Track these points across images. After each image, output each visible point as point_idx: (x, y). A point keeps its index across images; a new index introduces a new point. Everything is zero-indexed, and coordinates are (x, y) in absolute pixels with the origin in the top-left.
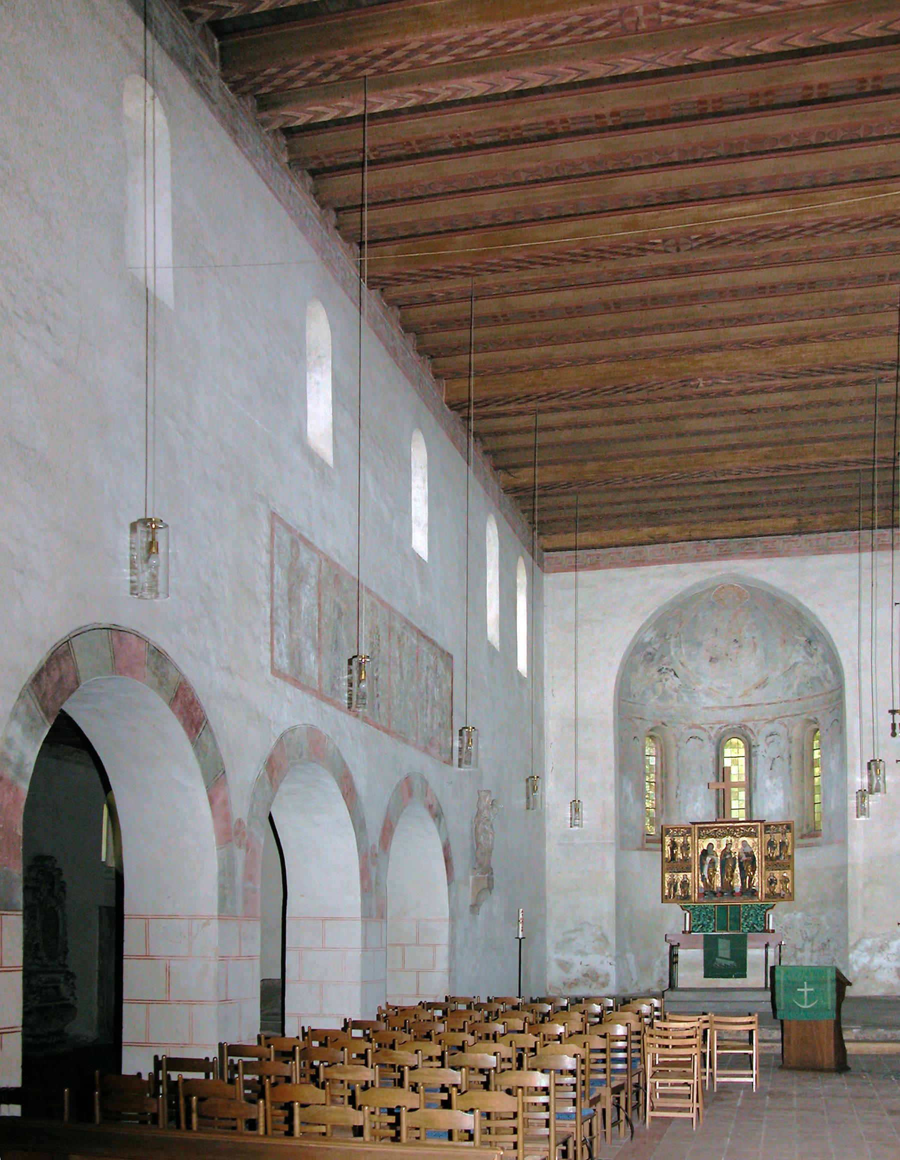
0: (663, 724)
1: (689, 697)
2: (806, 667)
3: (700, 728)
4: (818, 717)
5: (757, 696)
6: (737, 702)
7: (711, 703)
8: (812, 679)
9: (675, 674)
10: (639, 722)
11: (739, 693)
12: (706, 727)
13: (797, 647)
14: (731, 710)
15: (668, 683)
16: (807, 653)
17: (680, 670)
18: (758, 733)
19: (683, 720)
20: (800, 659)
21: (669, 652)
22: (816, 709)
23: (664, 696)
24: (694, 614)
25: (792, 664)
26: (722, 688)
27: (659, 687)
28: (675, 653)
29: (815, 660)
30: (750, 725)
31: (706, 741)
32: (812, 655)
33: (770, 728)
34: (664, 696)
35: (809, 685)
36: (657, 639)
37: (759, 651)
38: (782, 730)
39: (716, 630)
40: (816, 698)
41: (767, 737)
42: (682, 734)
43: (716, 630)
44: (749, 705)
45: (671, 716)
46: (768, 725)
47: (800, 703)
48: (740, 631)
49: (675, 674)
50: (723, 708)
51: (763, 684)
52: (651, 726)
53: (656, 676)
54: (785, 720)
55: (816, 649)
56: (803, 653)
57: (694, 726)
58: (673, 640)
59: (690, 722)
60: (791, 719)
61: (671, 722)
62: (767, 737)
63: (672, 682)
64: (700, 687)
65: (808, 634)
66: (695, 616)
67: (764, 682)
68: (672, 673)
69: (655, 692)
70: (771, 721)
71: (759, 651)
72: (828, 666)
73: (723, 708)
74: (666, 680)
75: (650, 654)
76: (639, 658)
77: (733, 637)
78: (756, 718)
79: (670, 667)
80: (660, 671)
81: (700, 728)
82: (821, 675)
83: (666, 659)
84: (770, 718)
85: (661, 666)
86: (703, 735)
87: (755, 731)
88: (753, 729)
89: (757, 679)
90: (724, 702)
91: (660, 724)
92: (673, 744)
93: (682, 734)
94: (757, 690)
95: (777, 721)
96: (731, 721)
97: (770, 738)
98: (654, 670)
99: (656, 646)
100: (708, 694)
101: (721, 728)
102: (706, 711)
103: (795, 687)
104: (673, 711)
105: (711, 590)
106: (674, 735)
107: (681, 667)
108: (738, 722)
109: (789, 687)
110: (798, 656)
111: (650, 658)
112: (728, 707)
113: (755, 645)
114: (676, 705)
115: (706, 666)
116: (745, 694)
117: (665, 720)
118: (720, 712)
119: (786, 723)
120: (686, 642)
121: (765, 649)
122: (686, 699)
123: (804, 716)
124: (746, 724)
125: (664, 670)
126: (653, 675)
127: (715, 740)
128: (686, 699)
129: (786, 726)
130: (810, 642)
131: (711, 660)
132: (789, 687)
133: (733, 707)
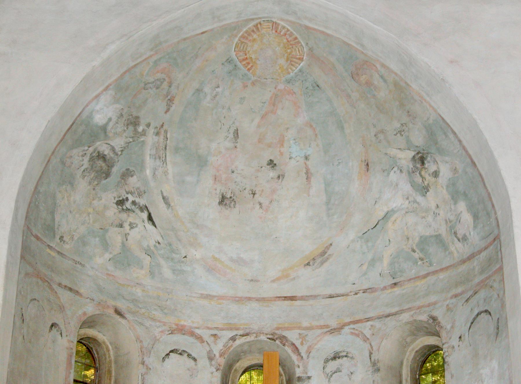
0: (118, 312)
1: (174, 271)
2: (411, 219)
3: (192, 334)
4: (438, 313)
5: (307, 281)
6: (269, 290)
7: (216, 287)
8: (424, 241)
9: (150, 218)
10: (65, 296)
11: (273, 273)
12: (205, 334)
13: (394, 176)
14: (254, 305)
15: (134, 234)
16: (413, 184)
17: (160, 211)
18: (309, 352)
19: (158, 314)
20: (398, 202)
21: (142, 166)
22: (433, 298)
23: (124, 259)
24: (196, 85)
25: (382, 214)
26: (239, 261)
27: (115, 237)
28: (155, 170)
29: (431, 200)
30: (293, 336)
31: (203, 362)
32: (424, 190)
33: (332, 344)
34: (124, 259)
35: (416, 255)
36: (120, 128)
37: (317, 185)
38: (358, 348)
39: (236, 133)
40: (432, 279)
41: (327, 361)
42: (156, 340)
43: (236, 133)
44: (292, 298)
45: (135, 301)
46: (328, 337)
47: (397, 290)
48: (281, 142)
49: (150, 218)
50: (239, 300)
51: (322, 256)
52: (90, 309)
53: (112, 212)
54: (366, 328)
55: (436, 174)
56: (406, 187)
57: (181, 330)
58: (150, 139)
59: (171, 320)
60: (377, 324)
61: (133, 313)
62: (327, 361)
63: (142, 234)
64: (196, 254)
65: (418, 139)
66: (199, 91)
67: (323, 253)
68: (145, 215)
69: (106, 245)
70: (333, 331)
71: (317, 185)
72: (462, 206)
73: (239, 300)
74: (132, 226)
75: (102, 157)
76: (80, 159)
77: (267, 155)
78: (305, 324)
79: (142, 202)
80: (121, 203)
81: (192, 334)
82: (443, 231)
83: (133, 181)
84: (334, 323)
85: (124, 196)
86: (198, 350)
87: (303, 350)
88: (298, 343)
89: (308, 248)
90: (243, 289)
91: (111, 311)
92: (136, 358)
93: (156, 340)
94: (309, 269)
95: (346, 329)
96: (255, 327)
97: (333, 365)
98: (109, 198)
99: (118, 143)
100: (211, 270)
101: (233, 339)
102: (205, 302)
103: (386, 262)
104: (139, 292)
105: (233, 28)
106: (138, 339)
107: (162, 205)
108: (268, 330)
109: (373, 263)
110: (394, 193)
111: (102, 166)
112: (249, 299)
113: (308, 175)
114: (148, 282)
115: (211, 211)
116: (285, 276)
117: (122, 305)
118: (234, 308)
119: (367, 333)
120: (177, 150)
121: (327, 184)
122: (167, 273)
123: (405, 317)
124: (285, 333)
125: (128, 205)
126: (106, 208)
127: (222, 361)
128: (167, 273)
129: (366, 339)
130: (422, 160)
131: (223, 200)
132: (373, 263)
133: (258, 300)
